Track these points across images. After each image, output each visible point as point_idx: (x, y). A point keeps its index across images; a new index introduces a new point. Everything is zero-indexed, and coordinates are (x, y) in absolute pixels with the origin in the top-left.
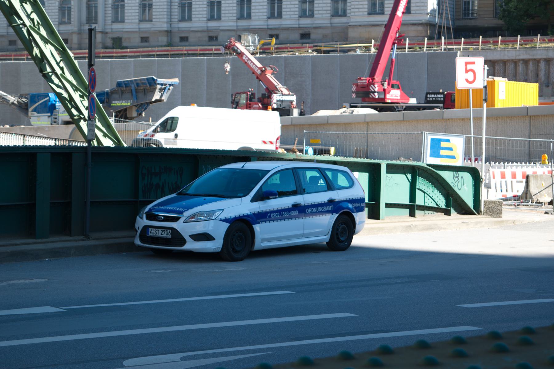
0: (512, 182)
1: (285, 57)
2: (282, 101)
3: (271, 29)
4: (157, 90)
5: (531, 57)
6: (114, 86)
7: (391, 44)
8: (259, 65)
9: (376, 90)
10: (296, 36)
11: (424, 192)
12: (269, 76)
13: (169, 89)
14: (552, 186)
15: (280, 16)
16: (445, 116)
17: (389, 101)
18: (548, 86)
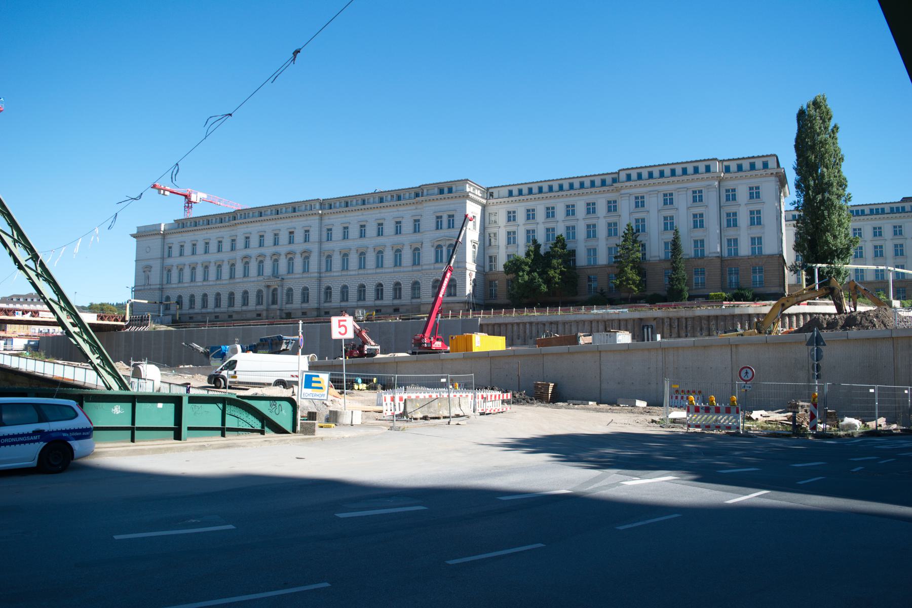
0: (399, 403)
2: (371, 349)
3: (377, 306)
4: (284, 343)
5: (522, 321)
6: (259, 341)
7: (436, 314)
9: (425, 342)
10: (391, 310)
11: (238, 418)
12: (364, 334)
13: (292, 343)
15: (382, 298)
17: (434, 349)
18: (519, 339)
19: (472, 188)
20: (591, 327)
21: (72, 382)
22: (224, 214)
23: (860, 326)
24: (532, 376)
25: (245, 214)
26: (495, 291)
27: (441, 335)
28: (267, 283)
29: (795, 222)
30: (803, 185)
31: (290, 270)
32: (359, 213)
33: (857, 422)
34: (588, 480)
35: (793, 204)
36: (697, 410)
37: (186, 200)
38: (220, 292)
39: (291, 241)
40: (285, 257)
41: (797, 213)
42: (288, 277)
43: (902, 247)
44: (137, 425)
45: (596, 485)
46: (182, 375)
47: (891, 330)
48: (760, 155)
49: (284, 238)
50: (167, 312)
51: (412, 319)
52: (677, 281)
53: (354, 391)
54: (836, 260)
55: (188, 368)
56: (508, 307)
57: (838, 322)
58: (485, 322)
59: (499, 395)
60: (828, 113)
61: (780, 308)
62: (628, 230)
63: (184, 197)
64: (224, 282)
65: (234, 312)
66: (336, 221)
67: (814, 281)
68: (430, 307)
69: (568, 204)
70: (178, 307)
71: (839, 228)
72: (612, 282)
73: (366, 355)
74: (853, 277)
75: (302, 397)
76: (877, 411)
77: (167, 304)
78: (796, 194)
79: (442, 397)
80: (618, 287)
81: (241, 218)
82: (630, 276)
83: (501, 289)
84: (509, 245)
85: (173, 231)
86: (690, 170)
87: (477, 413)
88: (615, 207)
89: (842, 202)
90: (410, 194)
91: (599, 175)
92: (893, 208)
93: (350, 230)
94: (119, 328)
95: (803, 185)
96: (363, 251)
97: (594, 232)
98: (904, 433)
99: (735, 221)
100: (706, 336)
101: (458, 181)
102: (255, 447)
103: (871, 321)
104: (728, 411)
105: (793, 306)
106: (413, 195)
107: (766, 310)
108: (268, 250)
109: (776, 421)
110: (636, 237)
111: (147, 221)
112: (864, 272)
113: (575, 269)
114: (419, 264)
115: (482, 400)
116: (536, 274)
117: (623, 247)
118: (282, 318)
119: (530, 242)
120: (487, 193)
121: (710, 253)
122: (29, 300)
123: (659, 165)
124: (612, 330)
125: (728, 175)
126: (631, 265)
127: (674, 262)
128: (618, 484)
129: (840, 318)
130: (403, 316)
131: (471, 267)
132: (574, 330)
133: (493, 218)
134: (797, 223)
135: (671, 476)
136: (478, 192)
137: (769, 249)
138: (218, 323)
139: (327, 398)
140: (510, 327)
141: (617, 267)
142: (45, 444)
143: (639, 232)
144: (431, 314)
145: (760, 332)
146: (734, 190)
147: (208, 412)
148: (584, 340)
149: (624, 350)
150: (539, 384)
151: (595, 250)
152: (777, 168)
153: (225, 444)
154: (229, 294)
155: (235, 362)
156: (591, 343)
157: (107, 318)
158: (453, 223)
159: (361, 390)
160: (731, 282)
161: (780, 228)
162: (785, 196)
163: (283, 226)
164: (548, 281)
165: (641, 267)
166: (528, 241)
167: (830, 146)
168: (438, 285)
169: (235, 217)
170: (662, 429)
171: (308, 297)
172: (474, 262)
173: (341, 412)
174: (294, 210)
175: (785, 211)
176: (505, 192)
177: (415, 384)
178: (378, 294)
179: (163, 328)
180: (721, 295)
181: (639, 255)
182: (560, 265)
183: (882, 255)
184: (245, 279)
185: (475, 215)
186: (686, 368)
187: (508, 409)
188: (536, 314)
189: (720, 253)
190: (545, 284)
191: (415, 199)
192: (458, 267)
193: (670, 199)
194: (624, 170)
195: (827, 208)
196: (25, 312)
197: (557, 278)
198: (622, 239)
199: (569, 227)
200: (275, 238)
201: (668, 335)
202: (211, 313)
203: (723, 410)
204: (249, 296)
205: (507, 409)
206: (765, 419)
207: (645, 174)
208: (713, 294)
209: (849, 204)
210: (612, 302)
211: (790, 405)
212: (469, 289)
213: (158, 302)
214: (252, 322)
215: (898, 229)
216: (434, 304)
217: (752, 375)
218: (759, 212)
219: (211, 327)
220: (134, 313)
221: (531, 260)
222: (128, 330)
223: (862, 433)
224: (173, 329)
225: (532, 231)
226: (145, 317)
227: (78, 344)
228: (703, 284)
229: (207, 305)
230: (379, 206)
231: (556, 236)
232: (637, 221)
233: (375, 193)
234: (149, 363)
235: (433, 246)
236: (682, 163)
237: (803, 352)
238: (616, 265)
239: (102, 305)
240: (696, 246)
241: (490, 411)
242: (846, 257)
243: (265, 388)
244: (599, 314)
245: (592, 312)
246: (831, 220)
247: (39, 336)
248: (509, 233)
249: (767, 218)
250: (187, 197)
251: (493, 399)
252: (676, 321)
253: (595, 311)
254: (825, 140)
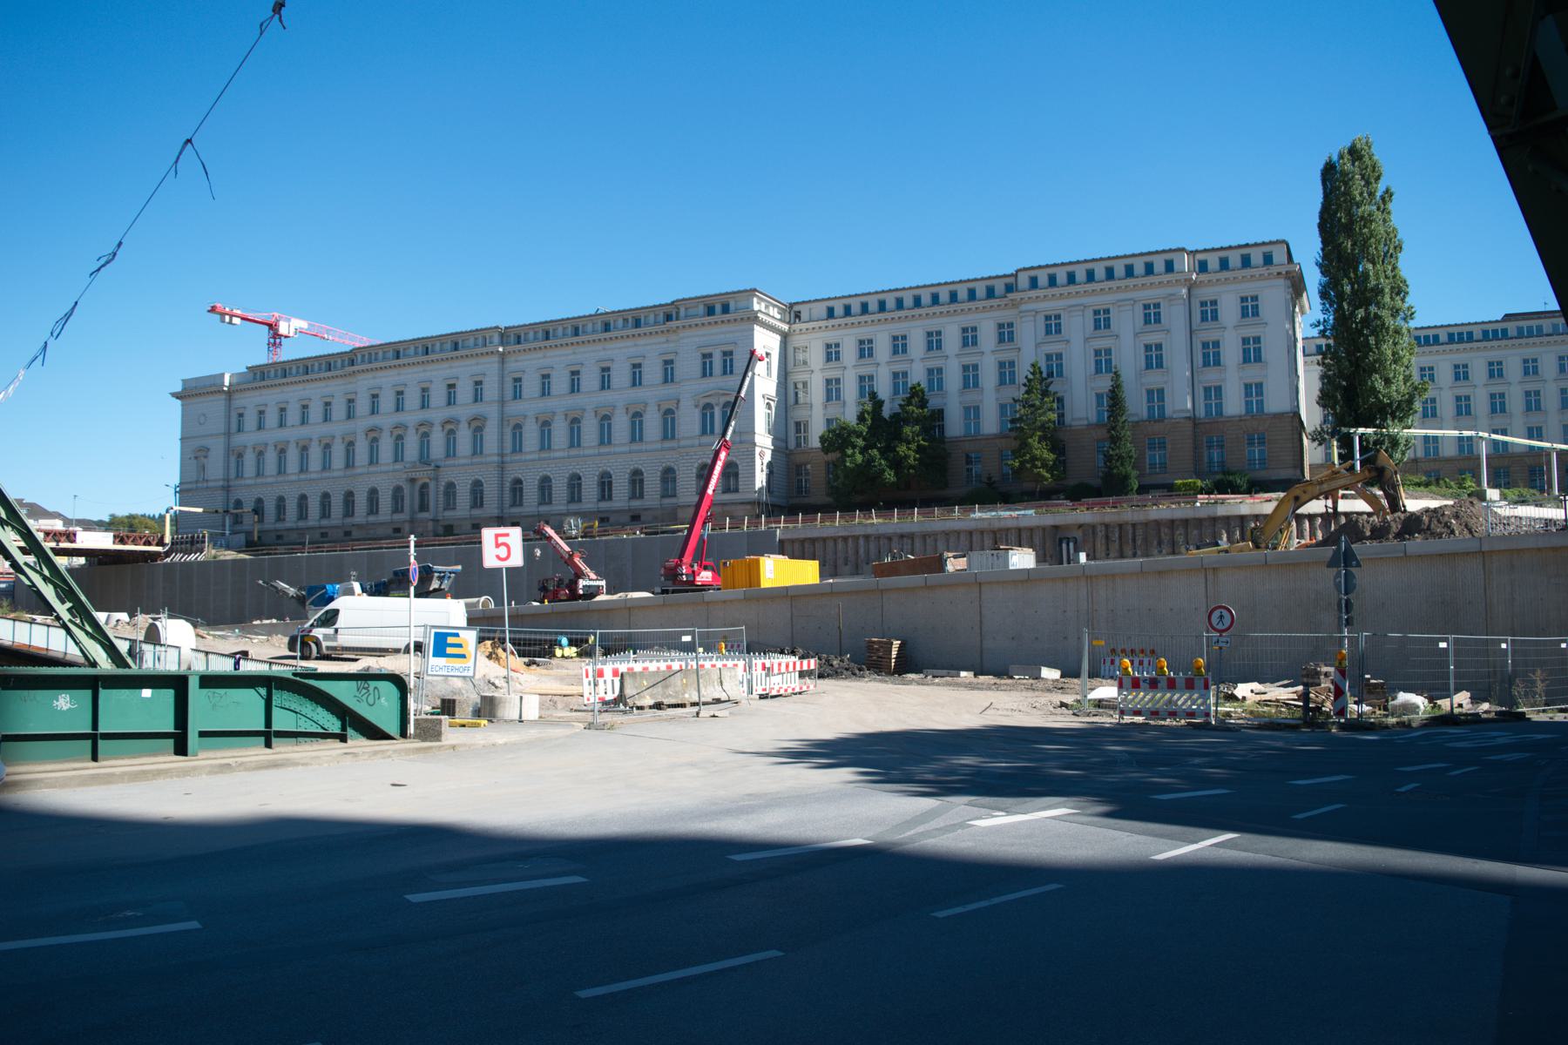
0: (613, 681)
1: (606, 540)
2: (589, 586)
4: (435, 579)
6: (391, 576)
8: (567, 549)
9: (684, 571)
10: (626, 518)
11: (296, 713)
12: (577, 560)
13: (449, 577)
15: (610, 498)
16: (706, 599)
17: (700, 584)
18: (846, 564)
19: (763, 304)
20: (968, 542)
21: (45, 652)
22: (333, 355)
23: (1428, 532)
24: (863, 628)
25: (370, 354)
26: (806, 481)
27: (711, 559)
28: (410, 474)
29: (1320, 357)
30: (1332, 293)
31: (451, 451)
32: (569, 350)
33: (1420, 701)
34: (909, 818)
35: (1316, 326)
36: (1136, 684)
37: (271, 332)
38: (480, 478)
39: (451, 401)
40: (441, 428)
41: (1323, 342)
42: (447, 463)
43: (1539, 395)
44: (101, 730)
45: (921, 829)
46: (248, 636)
47: (1480, 538)
48: (1259, 241)
49: (438, 396)
50: (238, 527)
51: (663, 533)
52: (1117, 460)
53: (554, 661)
54: (1390, 422)
55: (267, 624)
56: (828, 510)
57: (1389, 526)
58: (789, 536)
59: (795, 664)
60: (1374, 167)
61: (1292, 504)
62: (1033, 374)
63: (267, 328)
64: (336, 474)
65: (353, 525)
66: (528, 364)
67: (1352, 458)
68: (691, 511)
69: (929, 330)
70: (256, 520)
71: (1393, 366)
72: (1007, 464)
73: (581, 597)
74: (1420, 453)
75: (430, 673)
76: (1452, 682)
77: (237, 515)
78: (1321, 307)
79: (689, 667)
80: (1017, 472)
81: (363, 361)
82: (1038, 452)
83: (816, 475)
84: (830, 403)
85: (245, 386)
86: (1139, 268)
87: (755, 695)
88: (1011, 333)
89: (1399, 321)
90: (656, 316)
91: (983, 279)
92: (1453, 334)
93: (554, 380)
94: (154, 556)
95: (1332, 293)
96: (576, 416)
97: (976, 377)
98: (1502, 717)
99: (1217, 355)
100: (1168, 554)
101: (739, 292)
102: (326, 765)
103: (1446, 524)
104: (1190, 685)
105: (1314, 501)
106: (661, 317)
107: (1268, 508)
108: (412, 416)
109: (1277, 701)
110: (1048, 386)
111: (200, 369)
112: (1440, 441)
113: (944, 442)
114: (673, 437)
115: (764, 673)
116: (875, 452)
117: (1026, 404)
118: (438, 536)
119: (865, 396)
120: (790, 313)
121: (1174, 412)
123: (1047, 266)
124: (1001, 547)
125: (1204, 277)
126: (1039, 433)
127: (1113, 428)
128: (963, 825)
129: (1394, 520)
130: (646, 528)
131: (764, 442)
132: (941, 546)
133: (801, 356)
134: (1324, 358)
135: (1065, 807)
136: (774, 312)
137: (1275, 403)
138: (325, 545)
139: (474, 673)
140: (830, 544)
141: (1015, 439)
143: (1052, 376)
144: (692, 523)
145: (1257, 546)
146: (1214, 303)
147: (238, 703)
148: (954, 564)
149: (1022, 581)
150: (874, 642)
151: (977, 409)
152: (1288, 263)
153: (268, 761)
154: (368, 492)
155: (336, 612)
156: (966, 570)
157: (131, 539)
158: (731, 366)
159: (567, 658)
160: (1211, 461)
161: (1294, 367)
162: (1303, 313)
163: (437, 374)
164: (897, 464)
165: (1056, 438)
166: (862, 395)
167: (1379, 226)
168: (705, 473)
169: (353, 361)
170: (1076, 719)
171: (482, 498)
172: (769, 433)
173: (501, 698)
174: (456, 347)
175: (1303, 339)
176: (821, 309)
177: (661, 646)
178: (603, 490)
179: (230, 555)
180: (1195, 483)
181: (1053, 416)
182: (918, 436)
183: (1468, 413)
184: (373, 469)
185: (768, 351)
186: (1128, 610)
187: (812, 687)
188: (875, 521)
189: (1192, 411)
190: (891, 468)
191: (664, 324)
192: (741, 442)
193: (1211, 310)
194: (1025, 269)
195: (1374, 333)
197: (912, 459)
198: (1024, 389)
199: (898, 374)
200: (424, 396)
201: (1103, 554)
202: (336, 527)
203: (1180, 681)
204: (380, 497)
205: (808, 687)
206: (1258, 698)
207: (1062, 277)
208: (1180, 482)
209: (1412, 324)
210: (1007, 499)
211: (1305, 672)
212: (760, 479)
213: (220, 510)
214: (384, 543)
215: (1496, 368)
216: (698, 506)
217: (1229, 623)
218: (1257, 340)
219: (313, 552)
220: (181, 531)
221: (868, 428)
222: (168, 560)
223: (1426, 719)
224: (247, 557)
225: (869, 377)
226: (198, 537)
227: (34, 585)
228: (1163, 466)
229: (307, 514)
230: (602, 338)
231: (909, 385)
232: (1049, 357)
233: (596, 315)
234: (170, 617)
235: (696, 406)
236: (1125, 257)
237: (1326, 579)
238: (1014, 434)
239: (131, 517)
240: (1150, 400)
241: (779, 691)
242: (1406, 416)
243: (387, 658)
244: (984, 519)
245: (972, 516)
246: (1381, 353)
248: (828, 382)
249: (1272, 350)
250: (272, 327)
251: (783, 671)
252: (1117, 530)
253: (978, 515)
254: (1369, 215)
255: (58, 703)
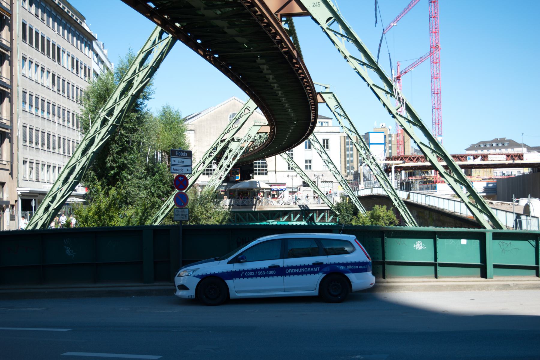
14: (322, 95)
122: (495, 145)
142: (324, 275)
196: (475, 157)
247: (495, 179)
255: (416, 246)
